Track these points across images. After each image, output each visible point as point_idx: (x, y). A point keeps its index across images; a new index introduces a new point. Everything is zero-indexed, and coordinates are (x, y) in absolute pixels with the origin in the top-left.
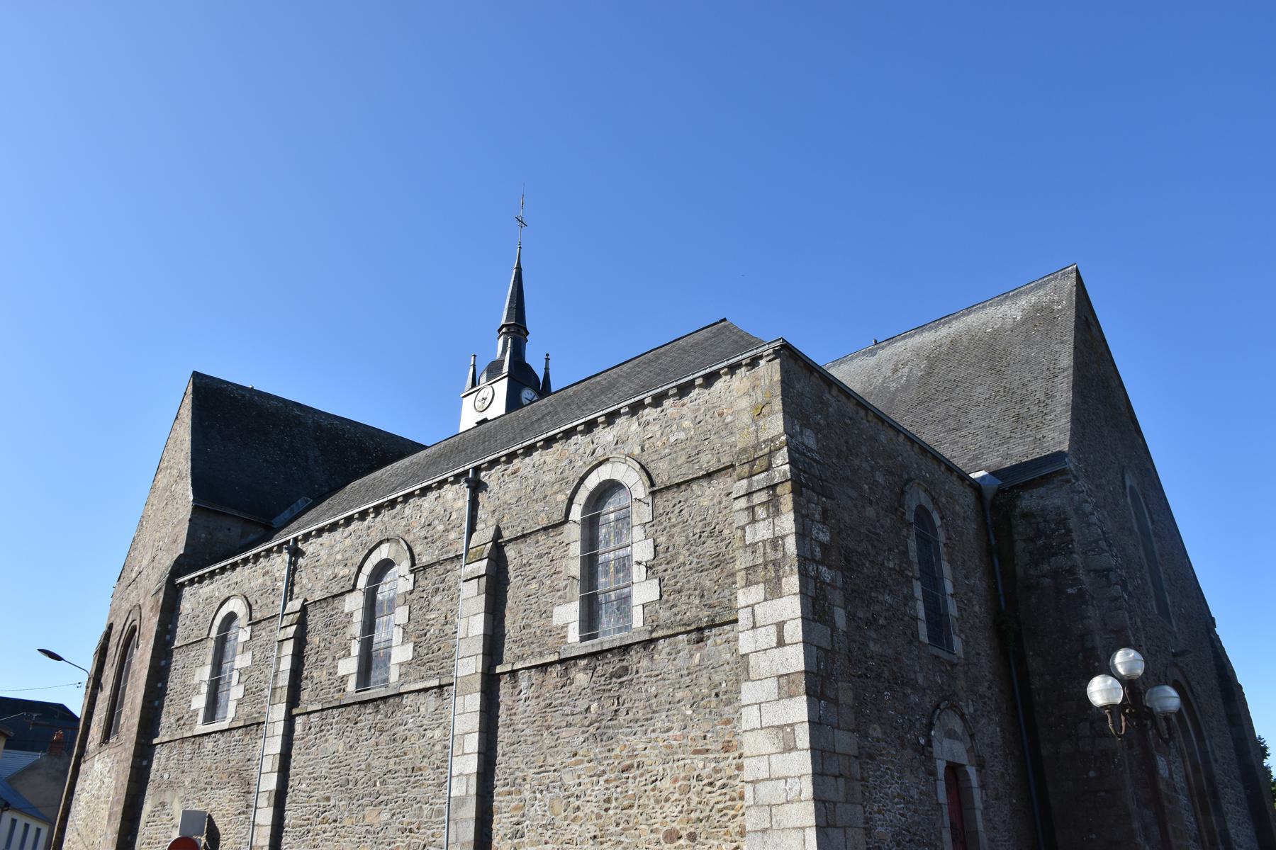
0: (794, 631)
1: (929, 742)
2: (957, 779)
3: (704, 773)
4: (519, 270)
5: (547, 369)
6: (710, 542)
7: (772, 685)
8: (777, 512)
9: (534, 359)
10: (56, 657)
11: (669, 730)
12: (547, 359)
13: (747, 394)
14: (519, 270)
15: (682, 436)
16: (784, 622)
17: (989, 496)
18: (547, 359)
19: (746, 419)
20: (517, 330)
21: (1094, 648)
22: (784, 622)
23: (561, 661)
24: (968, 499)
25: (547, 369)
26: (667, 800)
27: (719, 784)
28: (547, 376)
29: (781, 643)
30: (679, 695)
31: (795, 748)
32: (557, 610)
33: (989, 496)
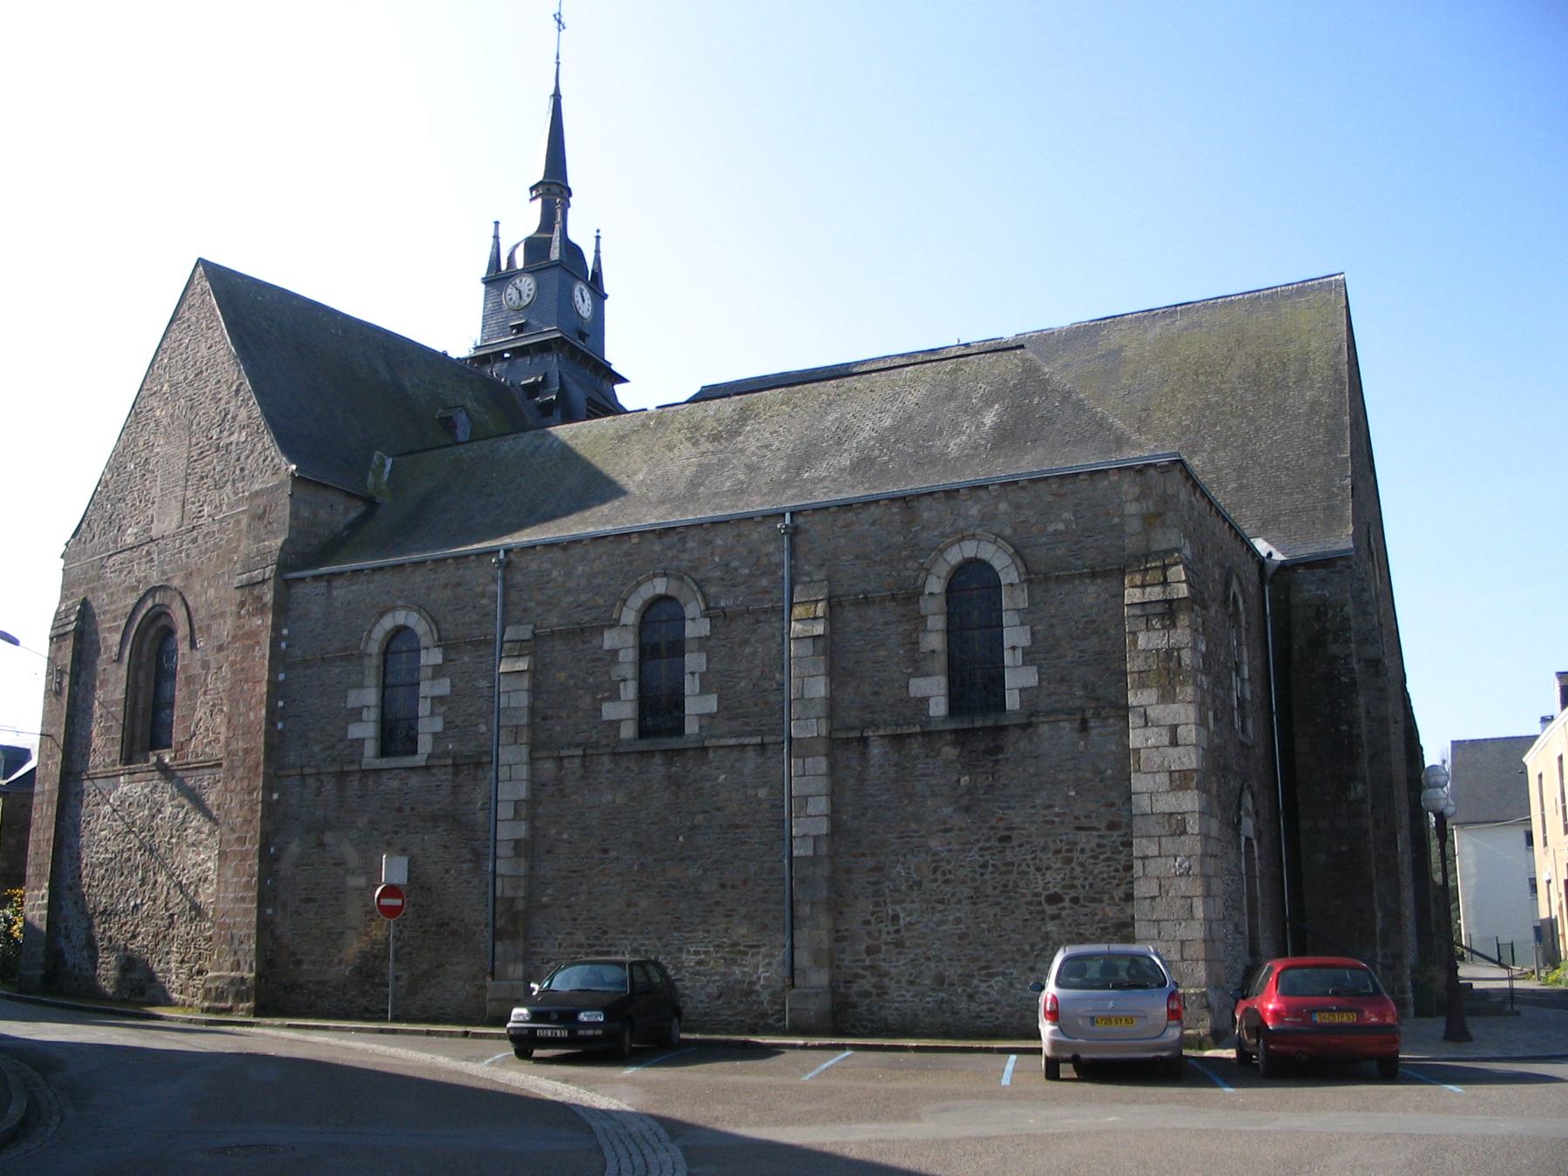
0: (1188, 733)
1: (1239, 821)
2: (70, 734)
3: (1088, 848)
4: (557, 97)
5: (597, 251)
6: (1095, 639)
7: (1163, 778)
8: (1174, 625)
9: (579, 231)
10: (14, 641)
11: (1051, 807)
12: (598, 238)
13: (1137, 499)
14: (557, 97)
15: (1061, 526)
16: (1176, 726)
17: (1270, 571)
18: (598, 238)
19: (1134, 526)
20: (554, 189)
21: (1358, 736)
22: (1176, 726)
23: (924, 734)
24: (1251, 569)
25: (597, 251)
26: (1048, 868)
27: (1103, 857)
28: (597, 260)
29: (1174, 742)
30: (1061, 777)
31: (1184, 832)
32: (913, 682)
33: (1270, 571)
